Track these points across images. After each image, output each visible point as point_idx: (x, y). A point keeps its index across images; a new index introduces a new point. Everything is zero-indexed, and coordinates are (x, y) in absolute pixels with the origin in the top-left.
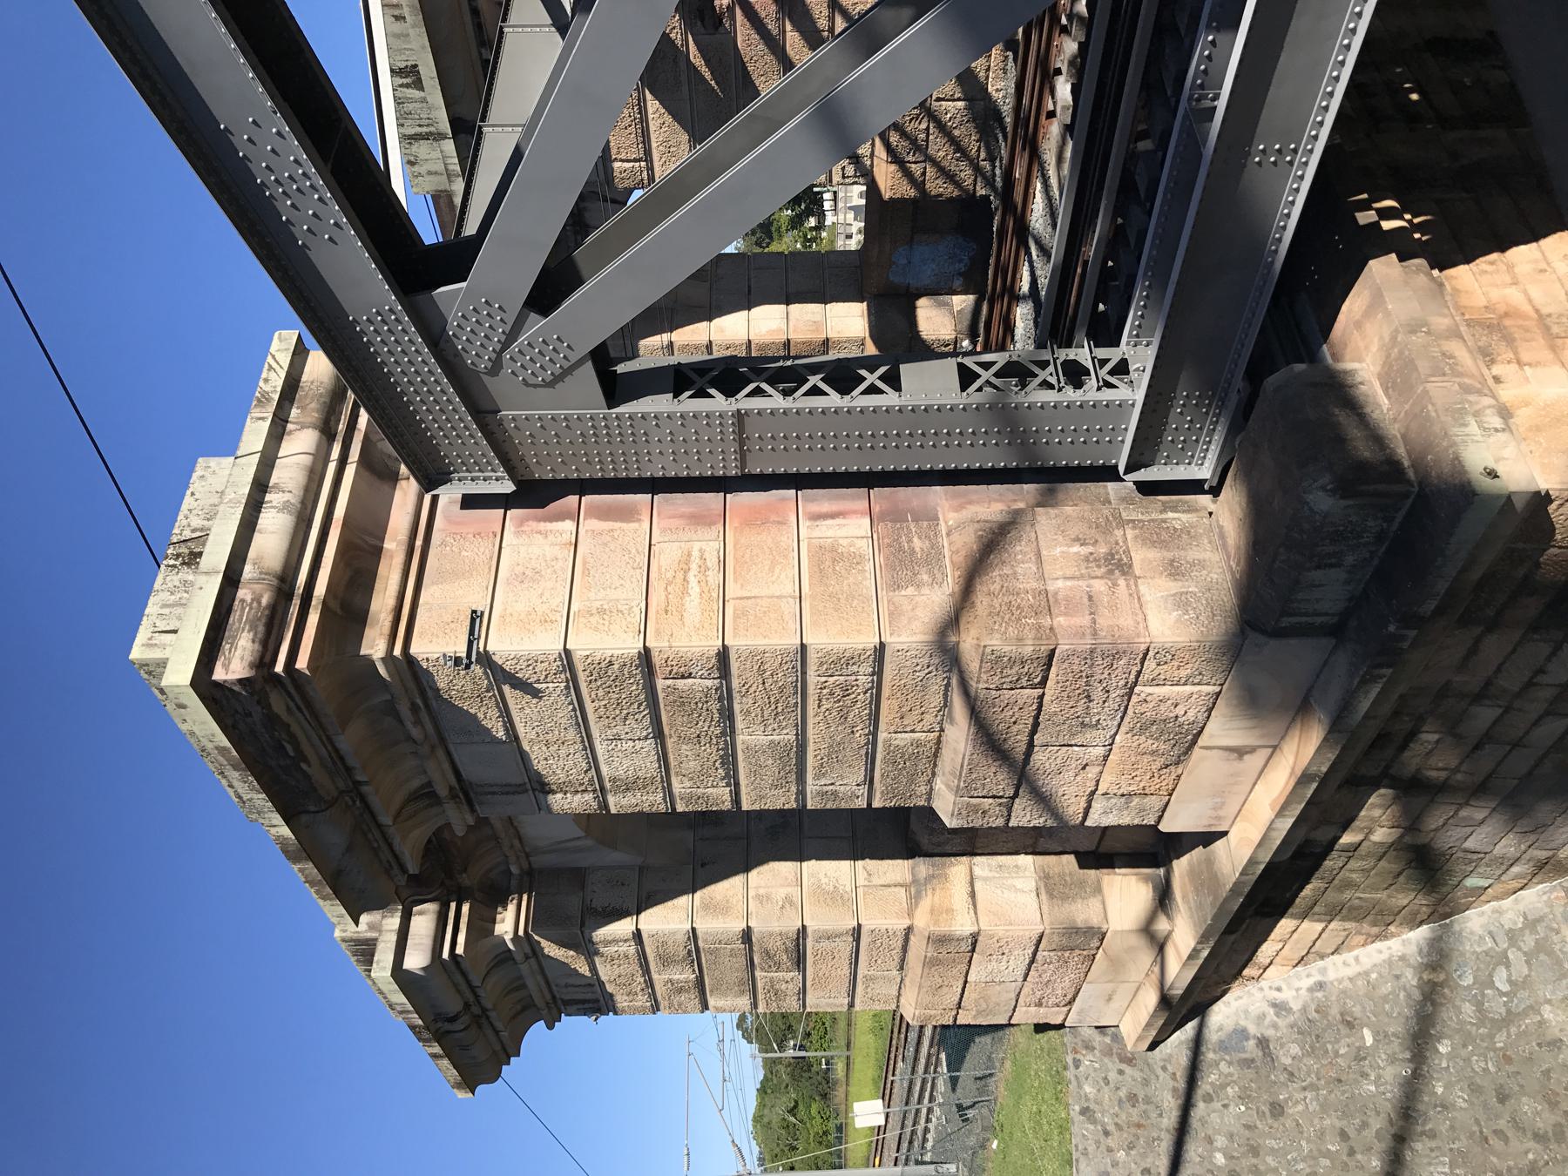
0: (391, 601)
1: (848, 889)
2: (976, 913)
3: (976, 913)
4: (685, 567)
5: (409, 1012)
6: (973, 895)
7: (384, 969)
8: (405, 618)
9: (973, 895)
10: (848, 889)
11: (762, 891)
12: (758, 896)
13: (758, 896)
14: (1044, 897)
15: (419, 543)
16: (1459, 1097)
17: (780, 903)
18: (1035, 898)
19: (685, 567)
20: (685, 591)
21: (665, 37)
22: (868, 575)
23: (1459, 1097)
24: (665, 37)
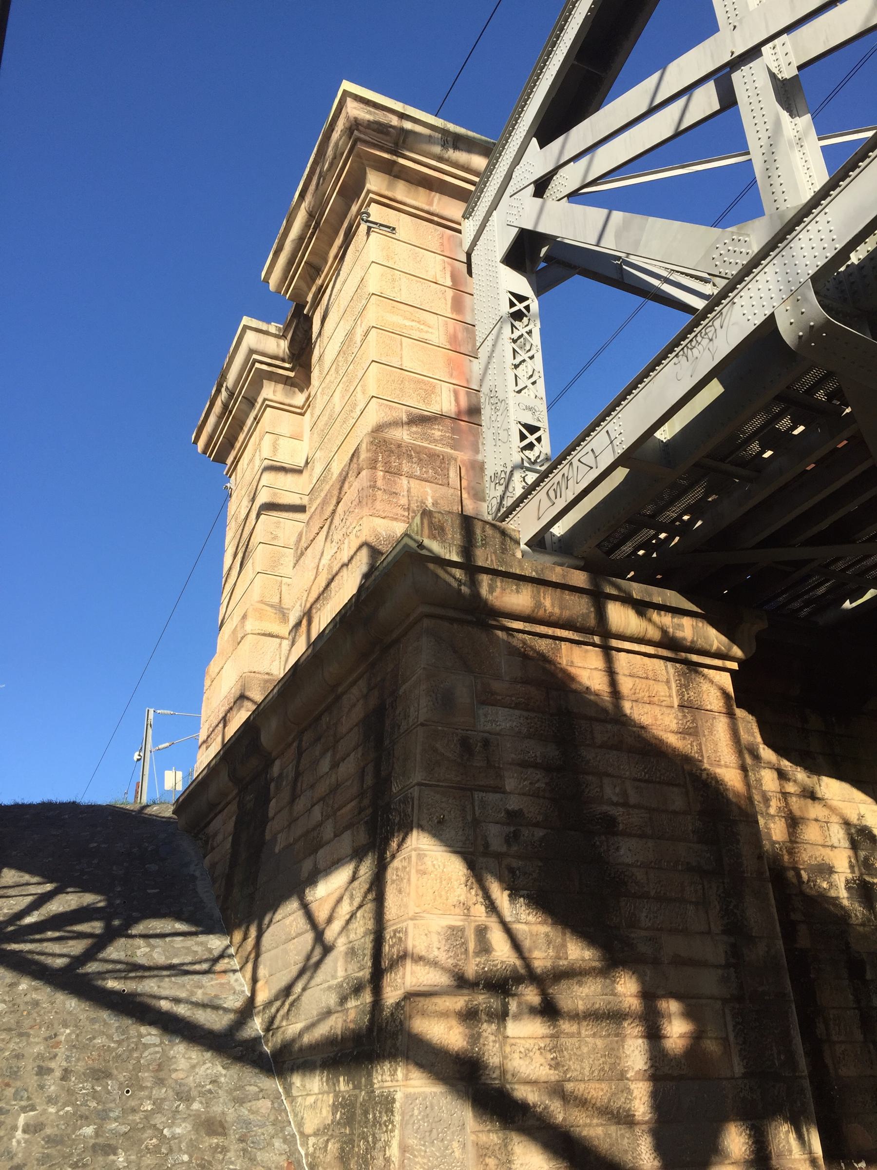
0: (399, 197)
1: (280, 571)
2: (259, 634)
3: (259, 634)
4: (422, 322)
5: (625, 1119)
6: (271, 635)
7: (248, 322)
8: (389, 203)
9: (271, 635)
10: (280, 571)
11: (282, 525)
12: (280, 522)
13: (280, 522)
14: (266, 677)
15: (436, 219)
16: (51, 1039)
17: (274, 533)
18: (267, 672)
19: (422, 322)
20: (406, 318)
21: (772, 317)
22: (416, 403)
23: (51, 1039)
24: (772, 317)
